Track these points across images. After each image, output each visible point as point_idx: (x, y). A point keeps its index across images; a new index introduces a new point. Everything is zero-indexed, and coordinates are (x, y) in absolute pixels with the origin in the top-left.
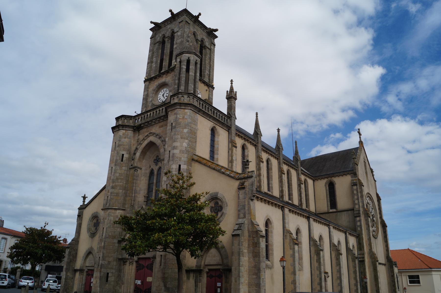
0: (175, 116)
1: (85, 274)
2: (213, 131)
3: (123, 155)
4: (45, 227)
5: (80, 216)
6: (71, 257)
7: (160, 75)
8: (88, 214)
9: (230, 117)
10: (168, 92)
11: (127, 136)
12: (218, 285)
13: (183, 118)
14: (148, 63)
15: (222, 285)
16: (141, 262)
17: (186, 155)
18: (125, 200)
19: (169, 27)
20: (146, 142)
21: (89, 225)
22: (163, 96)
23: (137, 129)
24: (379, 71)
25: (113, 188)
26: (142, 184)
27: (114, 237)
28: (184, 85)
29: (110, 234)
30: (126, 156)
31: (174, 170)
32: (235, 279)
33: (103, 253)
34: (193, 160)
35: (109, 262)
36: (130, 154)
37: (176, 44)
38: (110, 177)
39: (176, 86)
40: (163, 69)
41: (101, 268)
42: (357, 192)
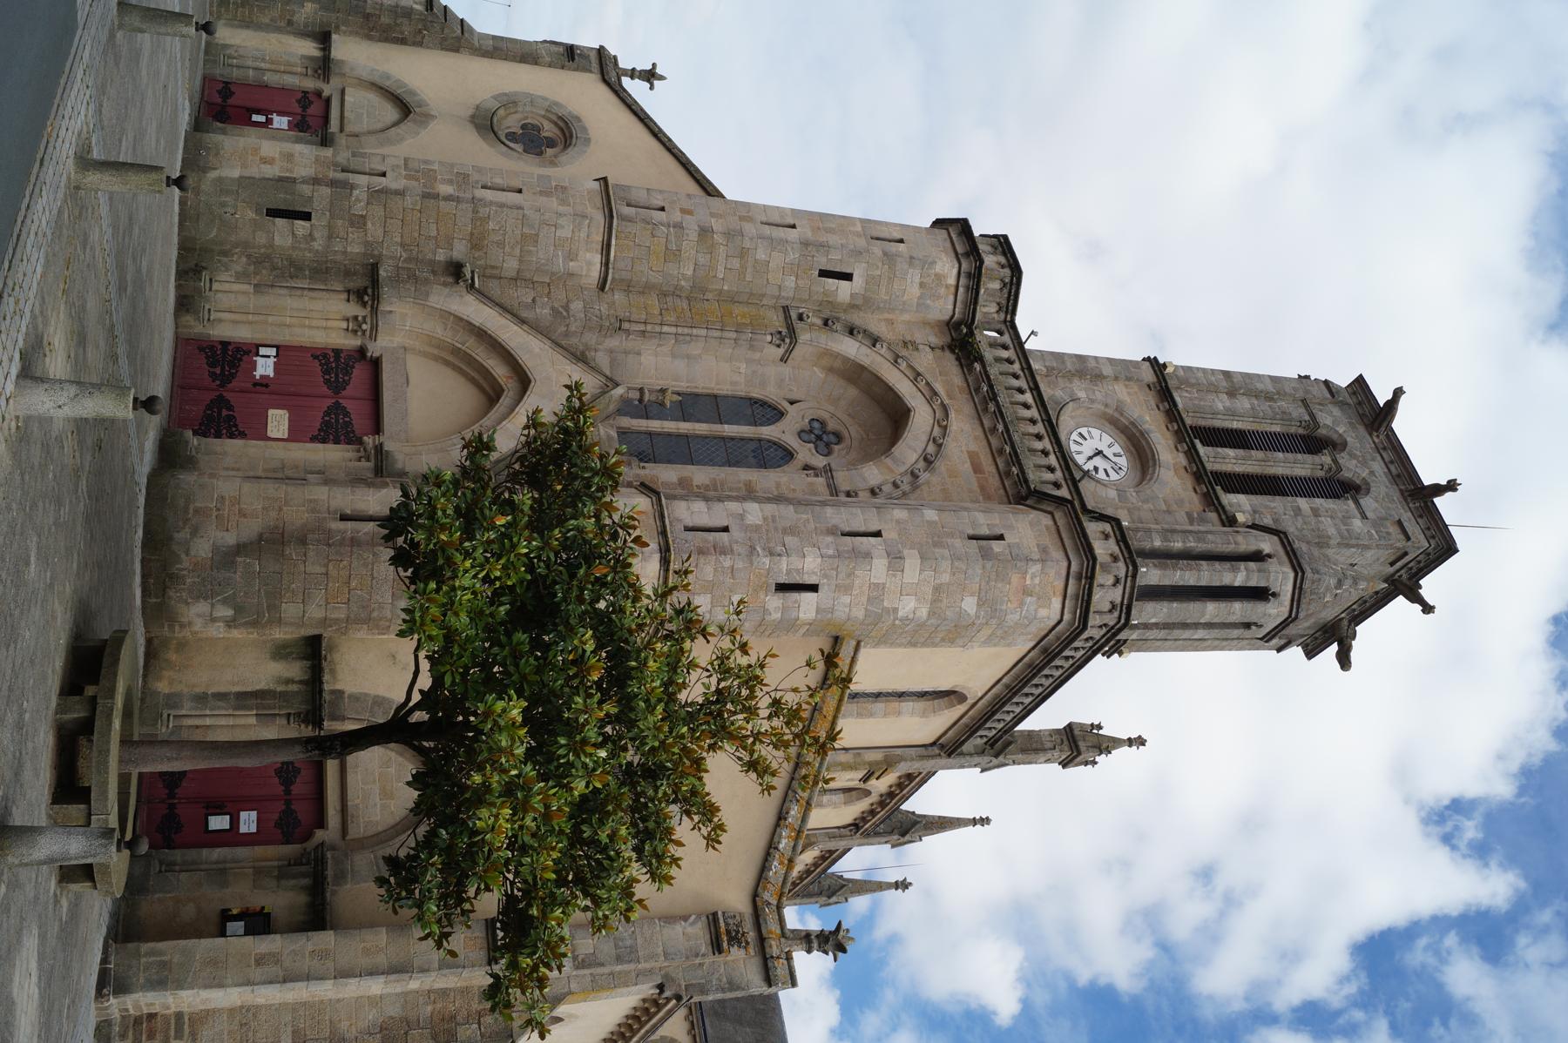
1: (310, 84)
2: (951, 696)
3: (847, 277)
5: (570, 55)
6: (385, 20)
7: (1192, 436)
8: (580, 93)
9: (992, 746)
10: (1114, 476)
11: (931, 292)
12: (244, 815)
13: (1026, 592)
14: (1227, 374)
15: (249, 840)
16: (359, 373)
17: (859, 613)
18: (647, 288)
19: (1378, 466)
20: (904, 388)
21: (532, 100)
22: (1093, 447)
23: (960, 340)
24: (1005, 1003)
25: (705, 232)
26: (718, 367)
27: (476, 243)
28: (1167, 582)
29: (491, 225)
30: (843, 290)
31: (796, 562)
32: (275, 958)
33: (401, 193)
35: (360, 222)
36: (853, 306)
37: (1316, 512)
38: (750, 219)
39: (1157, 543)
41: (333, 183)
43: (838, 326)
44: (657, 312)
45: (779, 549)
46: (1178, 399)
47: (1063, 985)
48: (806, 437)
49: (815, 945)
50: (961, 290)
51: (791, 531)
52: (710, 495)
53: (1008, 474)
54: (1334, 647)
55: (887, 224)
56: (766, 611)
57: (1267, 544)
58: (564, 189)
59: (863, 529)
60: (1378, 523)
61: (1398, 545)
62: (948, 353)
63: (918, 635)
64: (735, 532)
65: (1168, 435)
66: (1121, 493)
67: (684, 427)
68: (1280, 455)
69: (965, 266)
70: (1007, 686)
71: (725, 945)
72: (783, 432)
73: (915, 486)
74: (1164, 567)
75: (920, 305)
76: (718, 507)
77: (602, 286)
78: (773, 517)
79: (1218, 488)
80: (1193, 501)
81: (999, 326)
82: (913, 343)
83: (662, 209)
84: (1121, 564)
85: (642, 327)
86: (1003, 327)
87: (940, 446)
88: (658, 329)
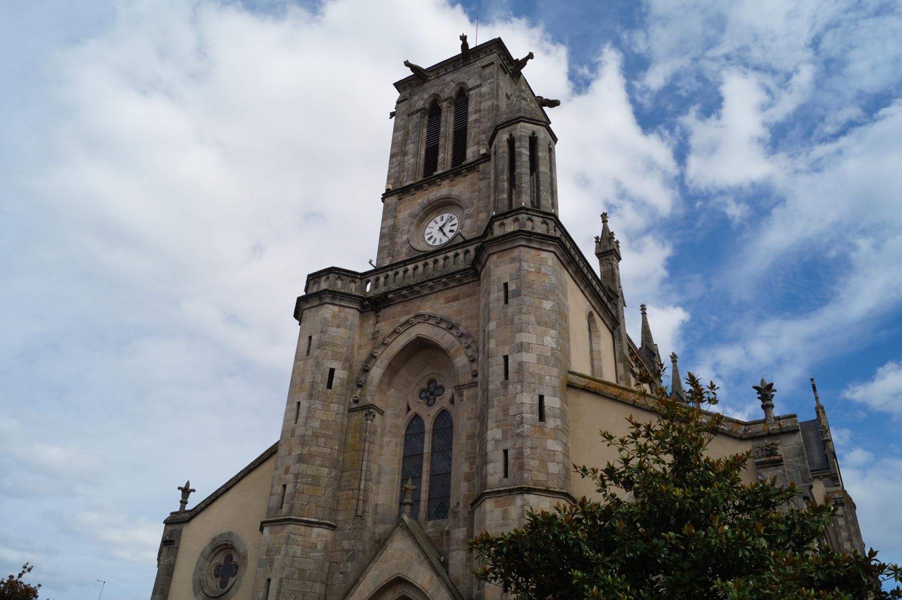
0: (518, 264)
3: (332, 371)
4: (20, 575)
5: (169, 544)
8: (197, 538)
9: (611, 299)
10: (456, 221)
11: (341, 323)
13: (538, 271)
14: (392, 156)
17: (555, 371)
18: (336, 499)
19: (448, 78)
21: (199, 569)
22: (437, 232)
23: (372, 306)
25: (301, 459)
26: (386, 455)
31: (526, 409)
34: (570, 386)
36: (350, 369)
37: (478, 111)
39: (505, 196)
40: (439, 167)
43: (362, 379)
44: (351, 493)
45: (518, 418)
46: (408, 183)
47: (668, 286)
48: (431, 402)
49: (769, 402)
50: (342, 303)
51: (505, 411)
52: (480, 460)
53: (460, 280)
54: (546, 109)
55: (299, 346)
56: (556, 428)
57: (504, 136)
58: (268, 550)
59: (503, 367)
60: (483, 78)
62: (381, 313)
63: (564, 337)
64: (508, 445)
65: (430, 190)
66: (468, 217)
67: (425, 477)
68: (442, 129)
69: (328, 301)
70: (585, 287)
71: (777, 458)
72: (429, 416)
74: (519, 194)
76: (491, 456)
77: (332, 527)
78: (496, 421)
80: (472, 177)
81: (364, 283)
82: (374, 334)
83: (285, 486)
84: (520, 216)
85: (361, 502)
86: (365, 280)
87: (441, 320)
88: (362, 492)
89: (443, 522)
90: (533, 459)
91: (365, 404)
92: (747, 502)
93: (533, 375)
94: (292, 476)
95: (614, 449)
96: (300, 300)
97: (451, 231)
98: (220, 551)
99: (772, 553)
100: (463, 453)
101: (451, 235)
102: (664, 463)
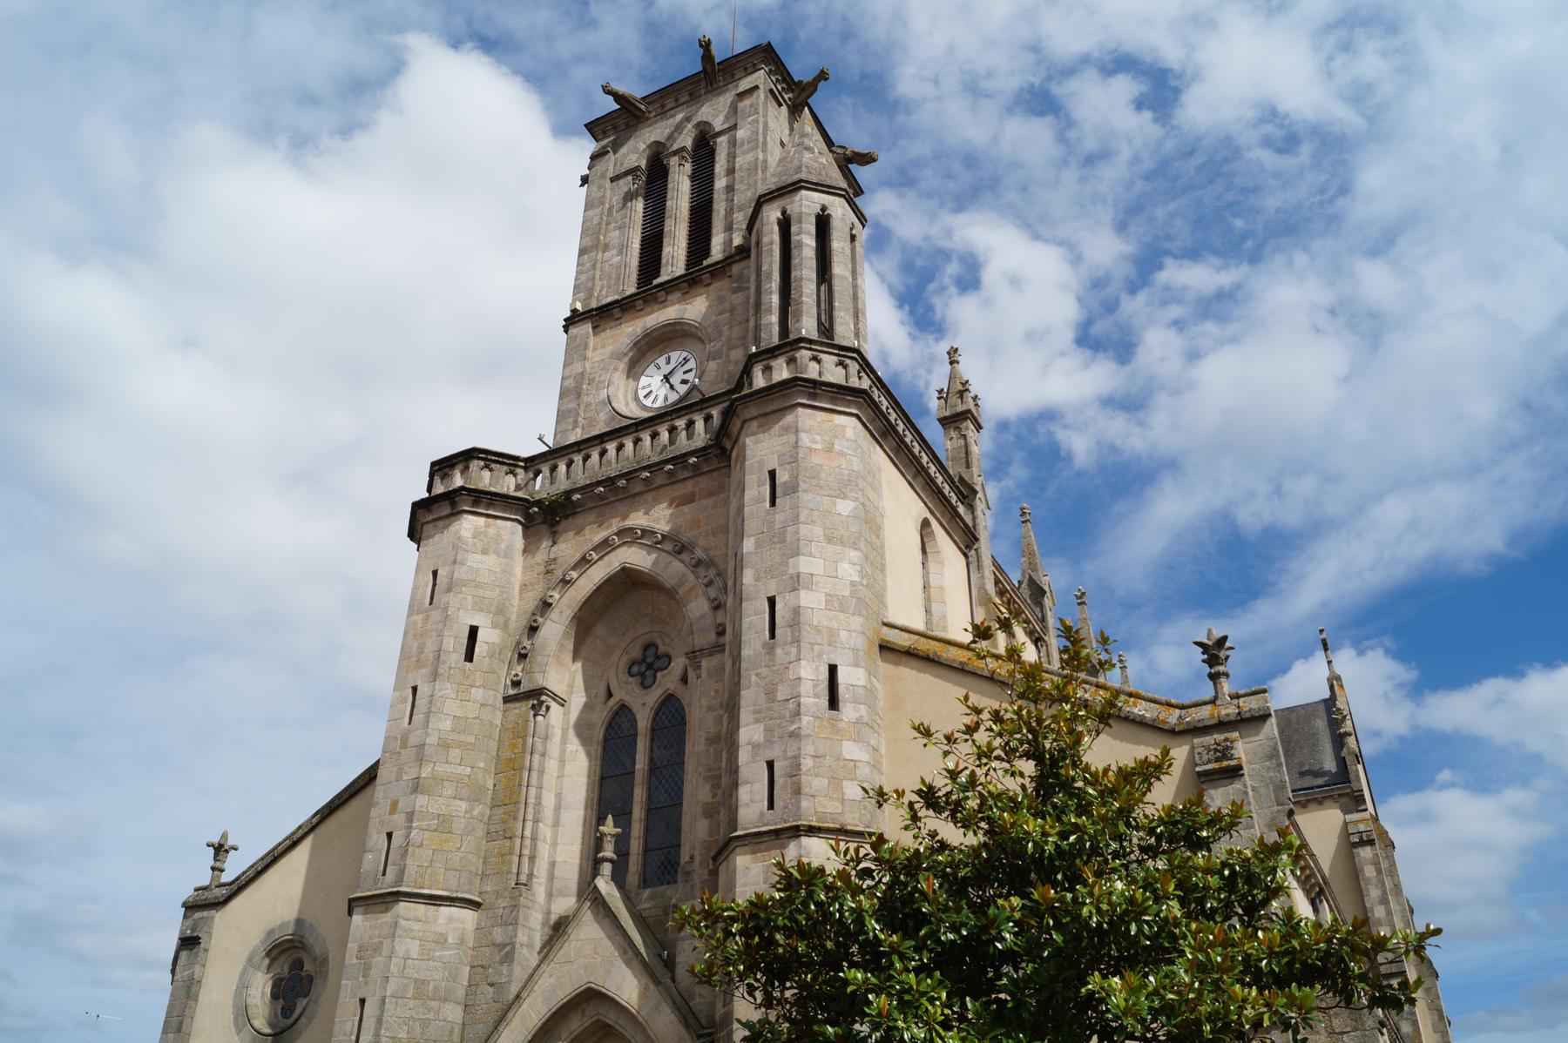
0: (792, 438)
3: (473, 631)
10: (692, 364)
11: (490, 548)
13: (830, 449)
17: (857, 622)
23: (544, 518)
26: (565, 773)
29: (402, 1035)
31: (805, 688)
42: (1379, 871)
43: (527, 643)
45: (791, 705)
46: (609, 300)
48: (648, 681)
49: (1221, 668)
51: (770, 694)
52: (726, 780)
56: (859, 722)
57: (772, 214)
61: (762, 96)
63: (874, 562)
65: (648, 310)
67: (638, 812)
70: (915, 477)
71: (1232, 763)
72: (644, 706)
73: (710, 563)
74: (798, 314)
75: (507, 555)
78: (755, 712)
79: (705, 263)
80: (721, 286)
83: (390, 835)
89: (668, 890)
90: (817, 775)
91: (532, 687)
92: (1159, 838)
93: (818, 630)
94: (403, 816)
95: (935, 752)
96: (418, 507)
97: (684, 382)
98: (283, 951)
99: (1194, 926)
100: (701, 769)
101: (683, 389)
102: (1022, 775)
